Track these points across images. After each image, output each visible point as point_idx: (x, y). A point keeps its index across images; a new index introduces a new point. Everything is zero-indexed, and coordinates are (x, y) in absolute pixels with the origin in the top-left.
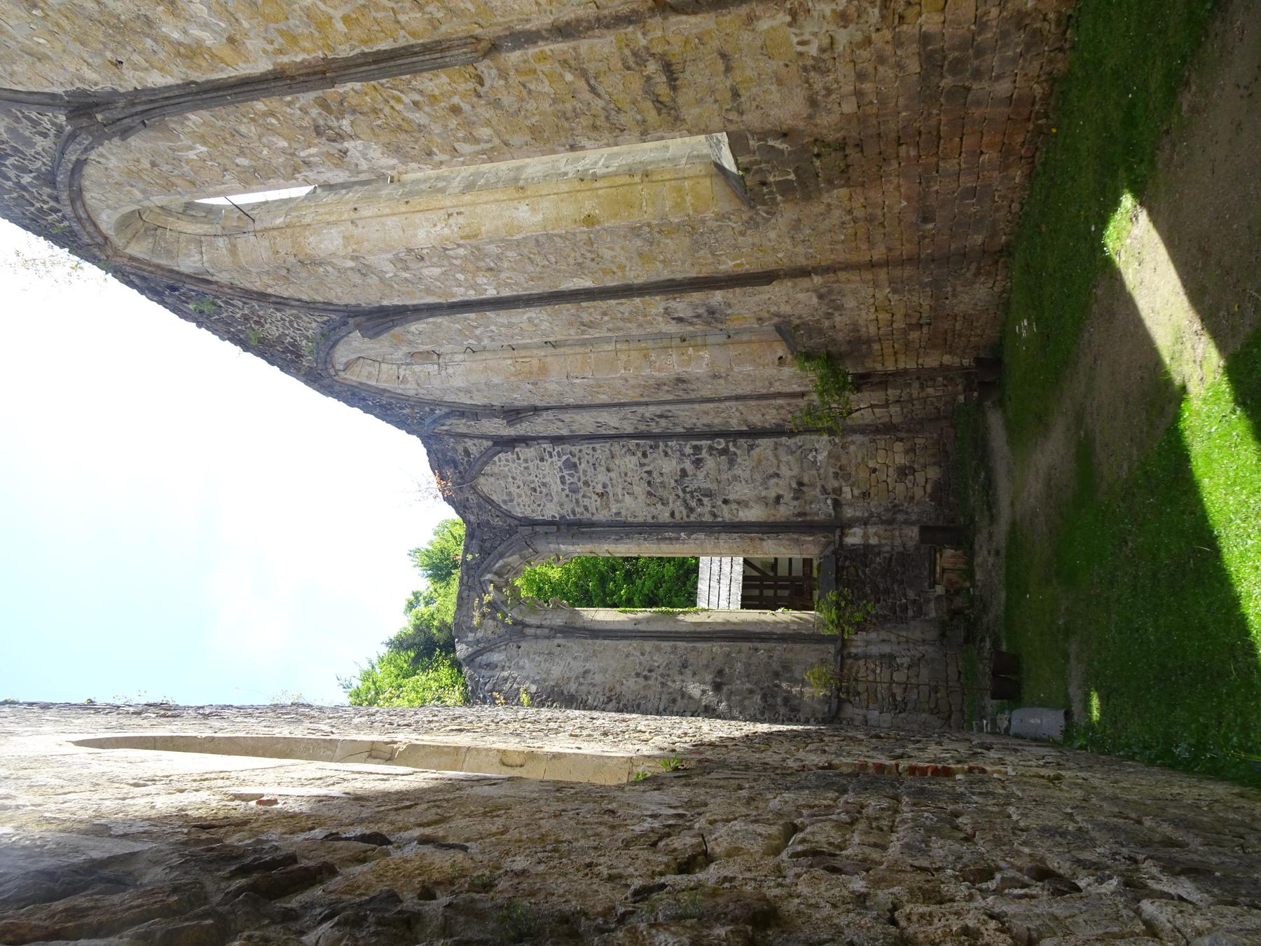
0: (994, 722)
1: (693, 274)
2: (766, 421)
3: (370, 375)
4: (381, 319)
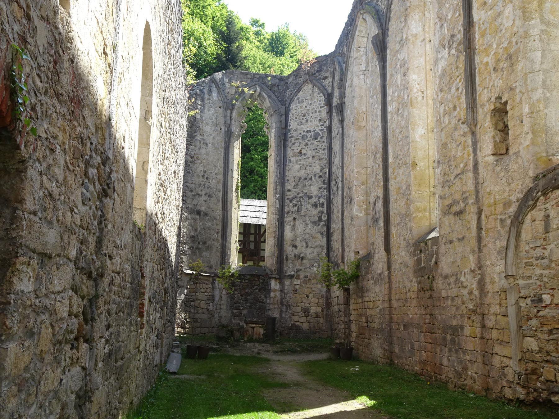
0: (178, 346)
1: (391, 213)
2: (334, 242)
3: (361, 31)
4: (381, 46)
